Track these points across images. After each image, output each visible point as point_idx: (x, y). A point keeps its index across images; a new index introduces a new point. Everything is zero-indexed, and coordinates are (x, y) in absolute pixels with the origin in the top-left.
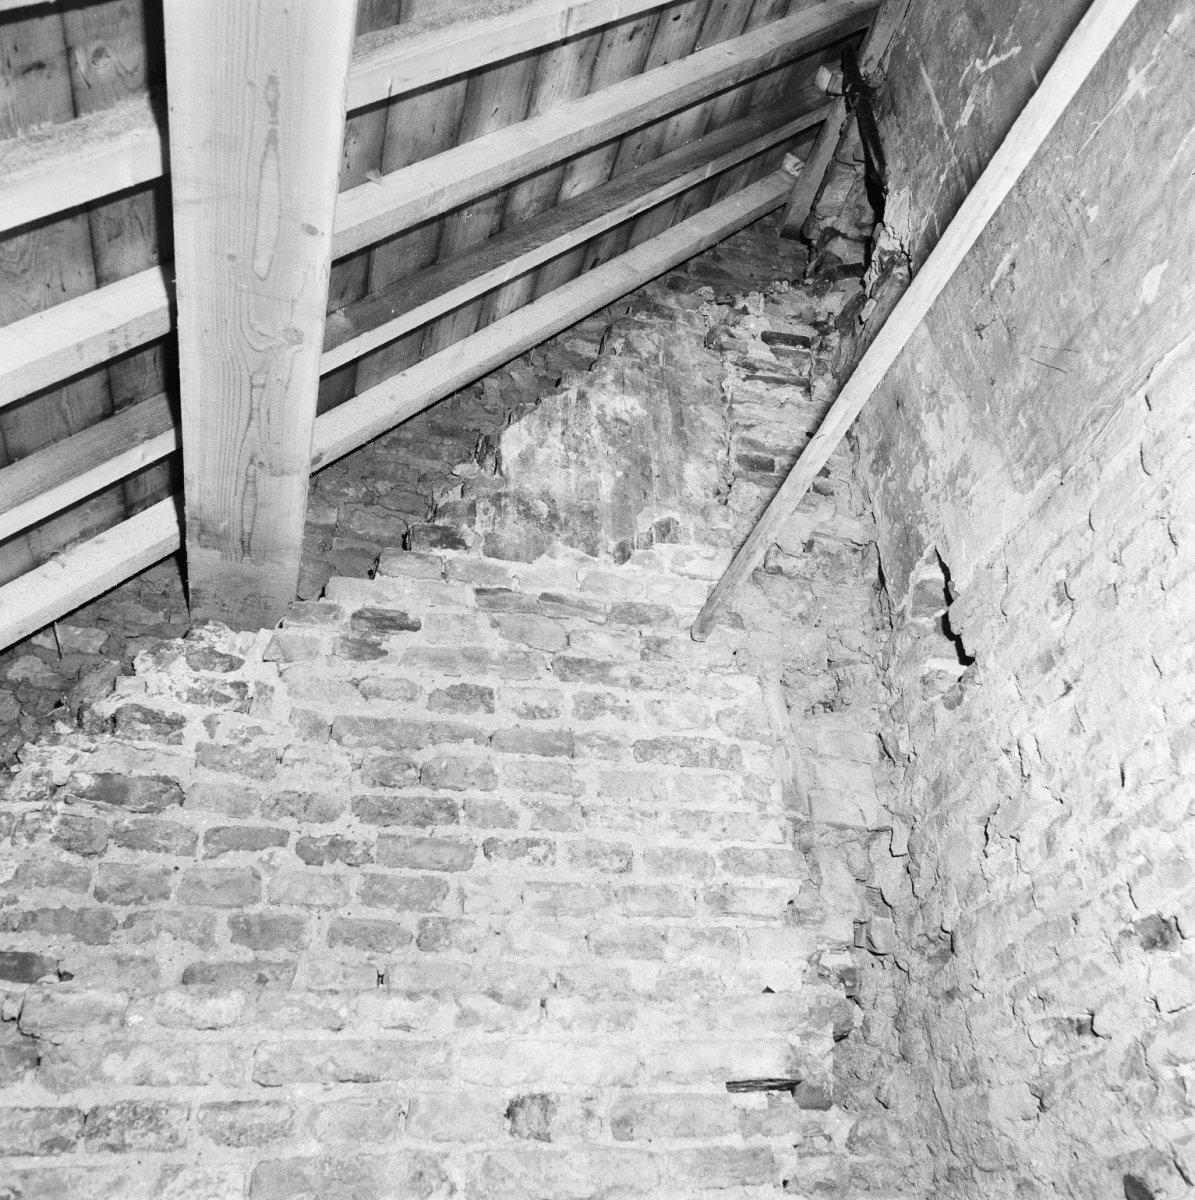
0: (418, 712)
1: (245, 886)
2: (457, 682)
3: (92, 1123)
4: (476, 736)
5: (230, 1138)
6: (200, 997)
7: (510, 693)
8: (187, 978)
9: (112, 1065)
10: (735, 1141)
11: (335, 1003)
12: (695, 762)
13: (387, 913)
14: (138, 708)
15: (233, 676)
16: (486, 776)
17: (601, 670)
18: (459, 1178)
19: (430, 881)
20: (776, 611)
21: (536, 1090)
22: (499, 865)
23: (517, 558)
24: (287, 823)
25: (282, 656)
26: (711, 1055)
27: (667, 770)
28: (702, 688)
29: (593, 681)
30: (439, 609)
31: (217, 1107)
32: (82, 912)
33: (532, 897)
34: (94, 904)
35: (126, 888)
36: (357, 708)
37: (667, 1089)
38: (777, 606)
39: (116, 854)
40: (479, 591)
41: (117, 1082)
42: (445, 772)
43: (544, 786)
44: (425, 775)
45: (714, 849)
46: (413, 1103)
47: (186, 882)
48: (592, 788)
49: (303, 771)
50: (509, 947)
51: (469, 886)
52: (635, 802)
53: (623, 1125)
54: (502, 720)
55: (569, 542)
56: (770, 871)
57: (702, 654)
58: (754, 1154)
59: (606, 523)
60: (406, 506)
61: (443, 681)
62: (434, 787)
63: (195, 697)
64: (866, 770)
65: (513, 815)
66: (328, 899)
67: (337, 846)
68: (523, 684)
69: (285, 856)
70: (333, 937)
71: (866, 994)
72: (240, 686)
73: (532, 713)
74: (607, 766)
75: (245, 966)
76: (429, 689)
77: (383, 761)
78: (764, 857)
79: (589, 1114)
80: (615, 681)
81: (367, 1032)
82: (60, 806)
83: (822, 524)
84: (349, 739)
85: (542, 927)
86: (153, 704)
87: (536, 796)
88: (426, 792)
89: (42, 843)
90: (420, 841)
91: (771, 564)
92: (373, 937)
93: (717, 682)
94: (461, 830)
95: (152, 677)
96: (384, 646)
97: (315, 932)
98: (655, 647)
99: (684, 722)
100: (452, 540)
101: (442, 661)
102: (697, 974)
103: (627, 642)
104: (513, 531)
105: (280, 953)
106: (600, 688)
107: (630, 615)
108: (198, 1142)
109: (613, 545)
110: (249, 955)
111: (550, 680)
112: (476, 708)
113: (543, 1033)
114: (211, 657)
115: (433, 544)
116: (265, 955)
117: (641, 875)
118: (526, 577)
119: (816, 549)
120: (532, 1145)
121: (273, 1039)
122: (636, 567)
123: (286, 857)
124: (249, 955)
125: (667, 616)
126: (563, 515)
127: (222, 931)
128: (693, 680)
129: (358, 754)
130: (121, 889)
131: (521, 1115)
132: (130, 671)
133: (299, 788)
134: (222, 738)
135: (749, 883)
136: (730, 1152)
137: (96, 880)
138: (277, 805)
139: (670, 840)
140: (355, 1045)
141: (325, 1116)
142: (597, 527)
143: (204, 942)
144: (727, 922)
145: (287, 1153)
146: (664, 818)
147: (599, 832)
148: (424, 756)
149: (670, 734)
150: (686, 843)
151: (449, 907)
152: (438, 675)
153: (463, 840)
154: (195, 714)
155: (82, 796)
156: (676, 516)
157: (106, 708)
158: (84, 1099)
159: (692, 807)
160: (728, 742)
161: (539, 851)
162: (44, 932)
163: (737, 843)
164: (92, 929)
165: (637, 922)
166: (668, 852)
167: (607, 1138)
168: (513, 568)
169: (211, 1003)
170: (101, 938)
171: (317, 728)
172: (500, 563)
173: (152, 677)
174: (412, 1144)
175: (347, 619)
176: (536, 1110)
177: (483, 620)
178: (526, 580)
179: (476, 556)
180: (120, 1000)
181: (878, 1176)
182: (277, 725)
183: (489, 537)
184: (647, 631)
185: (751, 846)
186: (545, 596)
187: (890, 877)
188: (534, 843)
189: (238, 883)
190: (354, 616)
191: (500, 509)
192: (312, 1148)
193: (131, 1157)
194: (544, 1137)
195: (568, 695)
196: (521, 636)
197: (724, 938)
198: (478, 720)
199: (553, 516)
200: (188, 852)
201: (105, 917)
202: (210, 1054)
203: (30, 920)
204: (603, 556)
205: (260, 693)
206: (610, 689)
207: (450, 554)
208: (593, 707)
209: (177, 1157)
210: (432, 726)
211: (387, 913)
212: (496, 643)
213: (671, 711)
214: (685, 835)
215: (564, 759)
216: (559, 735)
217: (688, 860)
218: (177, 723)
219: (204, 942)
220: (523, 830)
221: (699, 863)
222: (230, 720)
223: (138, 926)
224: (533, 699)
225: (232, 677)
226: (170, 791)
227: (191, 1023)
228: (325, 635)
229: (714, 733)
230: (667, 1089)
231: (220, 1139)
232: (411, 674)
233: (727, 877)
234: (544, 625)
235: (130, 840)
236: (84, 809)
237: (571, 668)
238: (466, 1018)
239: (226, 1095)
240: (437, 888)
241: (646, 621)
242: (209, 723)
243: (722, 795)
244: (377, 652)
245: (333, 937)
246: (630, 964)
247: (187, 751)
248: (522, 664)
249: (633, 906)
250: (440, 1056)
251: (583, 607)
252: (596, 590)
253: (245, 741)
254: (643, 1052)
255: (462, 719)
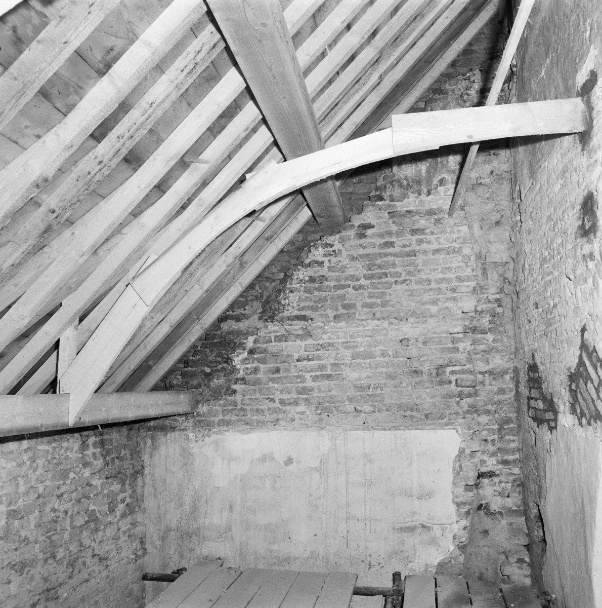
0: (377, 250)
1: (343, 297)
2: (385, 241)
3: (323, 346)
4: (391, 254)
5: (347, 348)
6: (337, 323)
7: (398, 241)
8: (335, 317)
9: (324, 336)
10: (450, 345)
11: (363, 322)
12: (448, 253)
13: (373, 300)
14: (314, 261)
15: (332, 249)
16: (394, 265)
17: (420, 231)
18: (391, 354)
19: (382, 292)
20: (479, 198)
21: (406, 337)
22: (398, 287)
23: (398, 201)
24: (349, 282)
25: (342, 241)
26: (445, 328)
27: (441, 256)
28: (451, 232)
29: (420, 235)
30: (379, 220)
31: (344, 343)
32: (312, 306)
33: (406, 293)
34: (314, 304)
35: (320, 300)
36: (362, 251)
37: (434, 335)
38: (479, 196)
39: (316, 293)
40: (389, 213)
41: (325, 339)
42: (384, 265)
43: (408, 266)
44: (380, 267)
45: (453, 276)
46: (381, 341)
47: (331, 298)
48: (420, 265)
49: (351, 269)
50: (401, 305)
51: (392, 292)
52: (432, 267)
53: (424, 343)
54: (397, 249)
55: (413, 193)
56: (468, 281)
57: (451, 221)
58: (454, 348)
59: (424, 183)
60: (370, 181)
61: (382, 241)
62: (382, 269)
63: (325, 256)
64: (506, 244)
65: (401, 274)
66: (360, 299)
67: (361, 286)
68: (402, 238)
69: (350, 290)
70: (363, 306)
71: (504, 304)
72: (334, 251)
73: (405, 246)
74: (425, 258)
75: (346, 314)
76: (378, 244)
77: (369, 265)
78: (466, 278)
79: (417, 341)
80: (426, 234)
81: (370, 327)
82: (303, 285)
83: (494, 167)
84: (361, 260)
85: (410, 300)
86: (316, 259)
87: (406, 268)
88: (380, 271)
89: (302, 293)
90: (379, 283)
91: (479, 182)
92: (371, 306)
93: (455, 229)
94: (389, 279)
95: (315, 252)
96: (366, 234)
97: (359, 306)
98: (438, 221)
99: (446, 243)
100: (381, 198)
101: (381, 236)
102: (447, 308)
103: (430, 221)
104: (397, 192)
105: (352, 311)
106: (422, 237)
107: (431, 212)
108: (341, 349)
109: (426, 190)
110: (346, 312)
111: (409, 236)
112: (390, 247)
113: (407, 326)
114: (327, 245)
115: (376, 201)
116: (349, 311)
117: (433, 285)
118: (401, 206)
119: (494, 174)
120: (405, 347)
121: (351, 330)
122: (433, 196)
123: (350, 290)
124: (346, 312)
125: (441, 211)
126: (411, 184)
127: (340, 307)
128: (448, 230)
129: (363, 263)
130: (319, 300)
131: (403, 342)
132: (310, 251)
133: (351, 274)
134: (333, 265)
135: (462, 284)
136: (449, 347)
137: (313, 299)
138: (347, 279)
139: (441, 276)
140: (368, 330)
141: (364, 344)
142: (421, 185)
143: (337, 310)
144: (455, 295)
145: (358, 350)
146: (440, 270)
147: (423, 276)
148: (378, 262)
149: (442, 246)
150: (445, 276)
151: (388, 298)
152: (380, 239)
153: (389, 282)
154: (325, 259)
155: (307, 282)
156: (445, 176)
157: (307, 261)
158: (321, 342)
159: (447, 266)
160: (458, 246)
161: (408, 282)
162: (307, 311)
163: (459, 274)
164: (315, 309)
165: (432, 297)
166: (440, 279)
167: (421, 346)
168: (398, 204)
169: (340, 324)
170: (317, 311)
171: (353, 258)
172: (394, 203)
173: (315, 252)
174: (381, 348)
175: (356, 228)
176: (406, 341)
177: (390, 221)
178: (401, 207)
179: (387, 202)
180: (323, 324)
181: (500, 348)
182: (344, 259)
183: (391, 196)
184: (436, 217)
185: (463, 275)
186: (407, 211)
187: (509, 275)
188: (406, 280)
189: (342, 297)
190: (358, 227)
191: (393, 186)
192: (362, 349)
193: (330, 352)
194: (408, 346)
195: (414, 240)
196: (401, 225)
197: (454, 299)
198: (391, 250)
199: (408, 185)
200: (330, 291)
201: (317, 306)
202: (341, 334)
203: (303, 308)
204: (423, 195)
205: (339, 252)
206: (425, 236)
207: (380, 203)
208: (421, 242)
209: (338, 352)
210: (380, 254)
211: (373, 300)
212: (394, 228)
213: (442, 240)
214: (445, 274)
215: (413, 258)
216: (411, 251)
217: (445, 280)
218: (322, 262)
219: (337, 310)
220: (404, 277)
221: (448, 280)
222: (334, 260)
223: (323, 308)
224: (404, 242)
225: (332, 249)
226: (324, 278)
227: (336, 328)
228: (351, 233)
229: (454, 244)
230: (434, 335)
231: (345, 348)
232: (373, 240)
233: (456, 283)
234: (407, 220)
235: (319, 290)
236: (308, 285)
237: (414, 232)
238: (390, 323)
239: (345, 341)
240: (384, 293)
241: (435, 214)
242: (329, 261)
243: (456, 261)
244: (364, 236)
245: (363, 306)
246: (430, 307)
247: (326, 268)
248: (400, 233)
249: (431, 293)
250: (385, 332)
251: (417, 213)
252: (422, 206)
253: (338, 265)
254: (429, 328)
255: (387, 250)
